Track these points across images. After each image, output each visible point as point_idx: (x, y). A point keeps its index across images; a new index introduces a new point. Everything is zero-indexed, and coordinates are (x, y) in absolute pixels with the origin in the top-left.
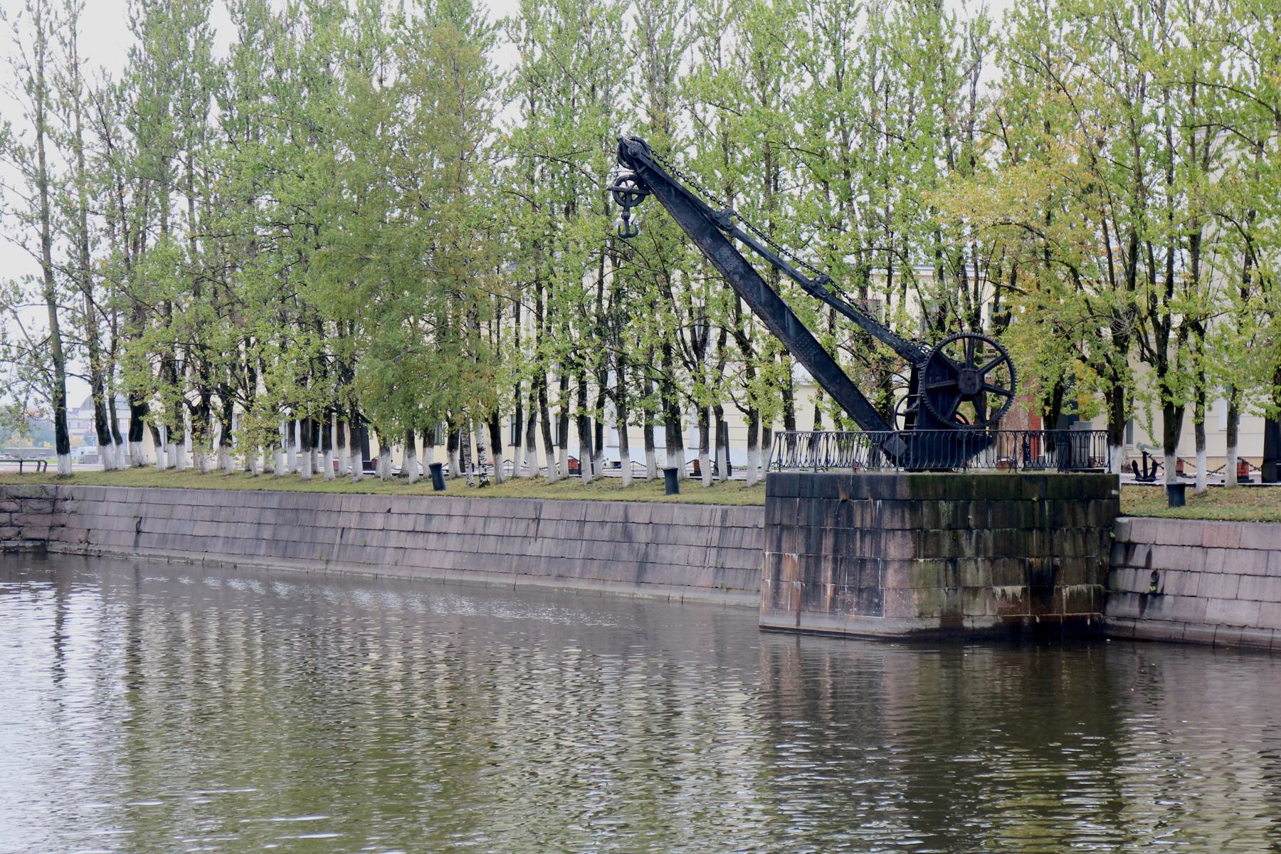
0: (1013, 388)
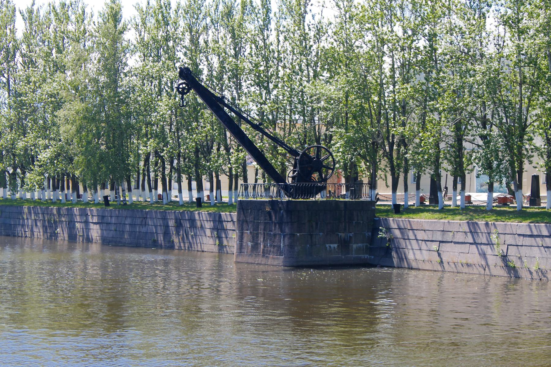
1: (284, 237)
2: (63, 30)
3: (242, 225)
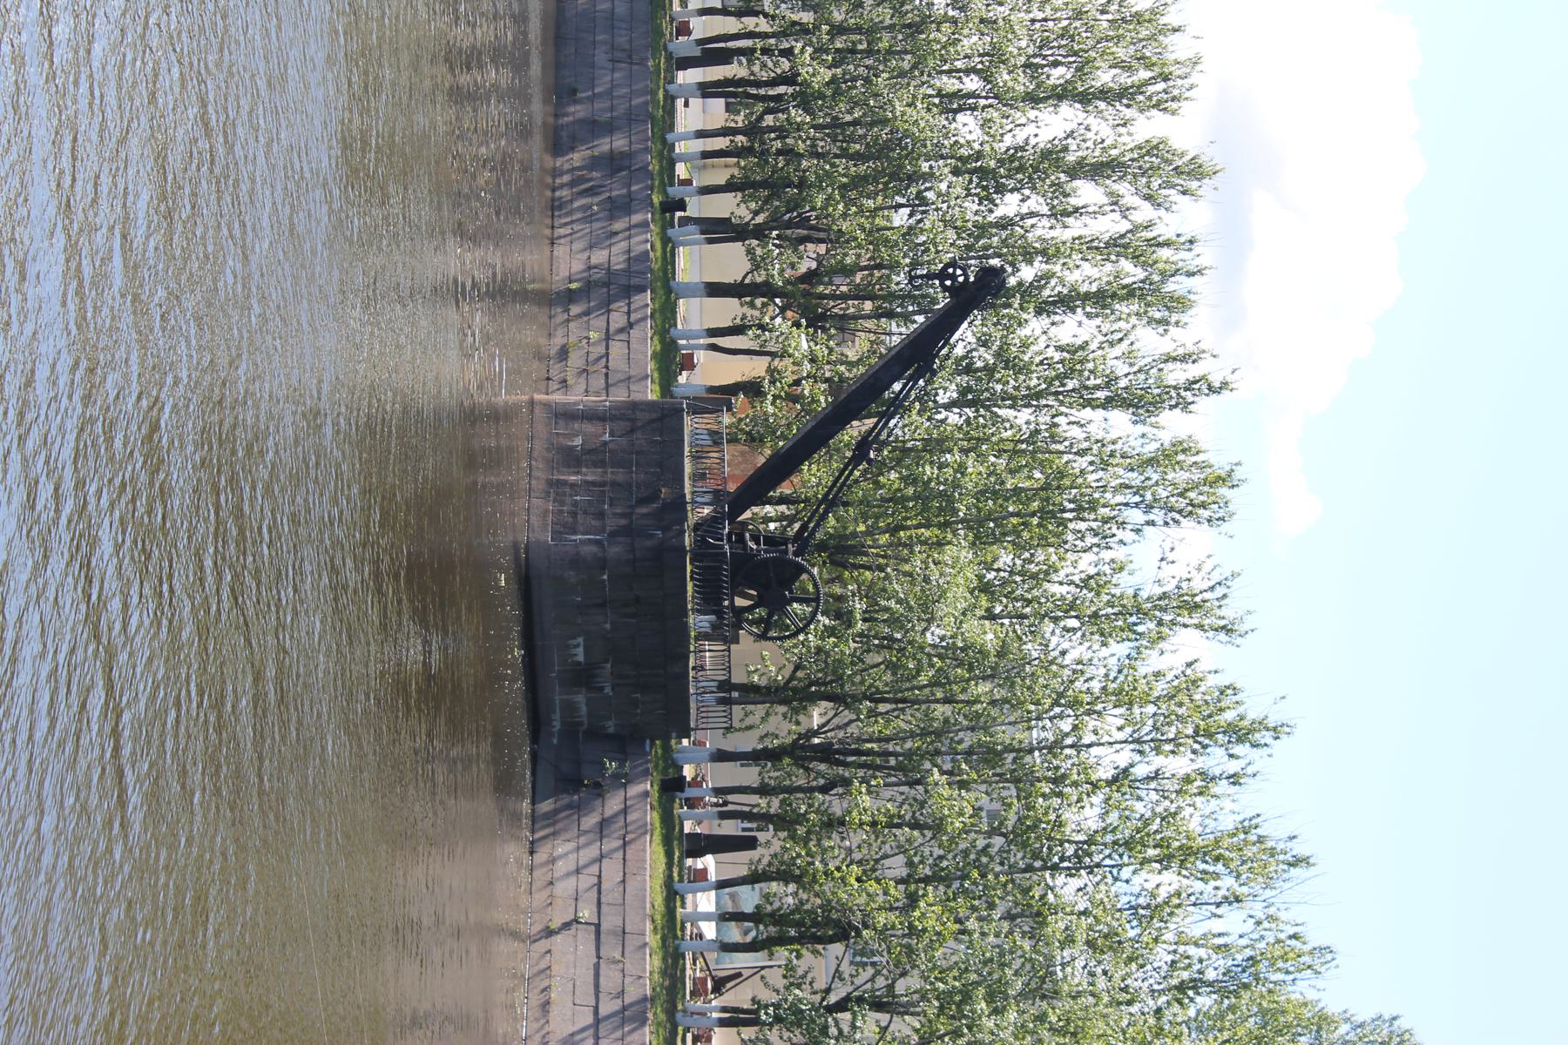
0: (772, 639)
1: (597, 542)
3: (622, 418)
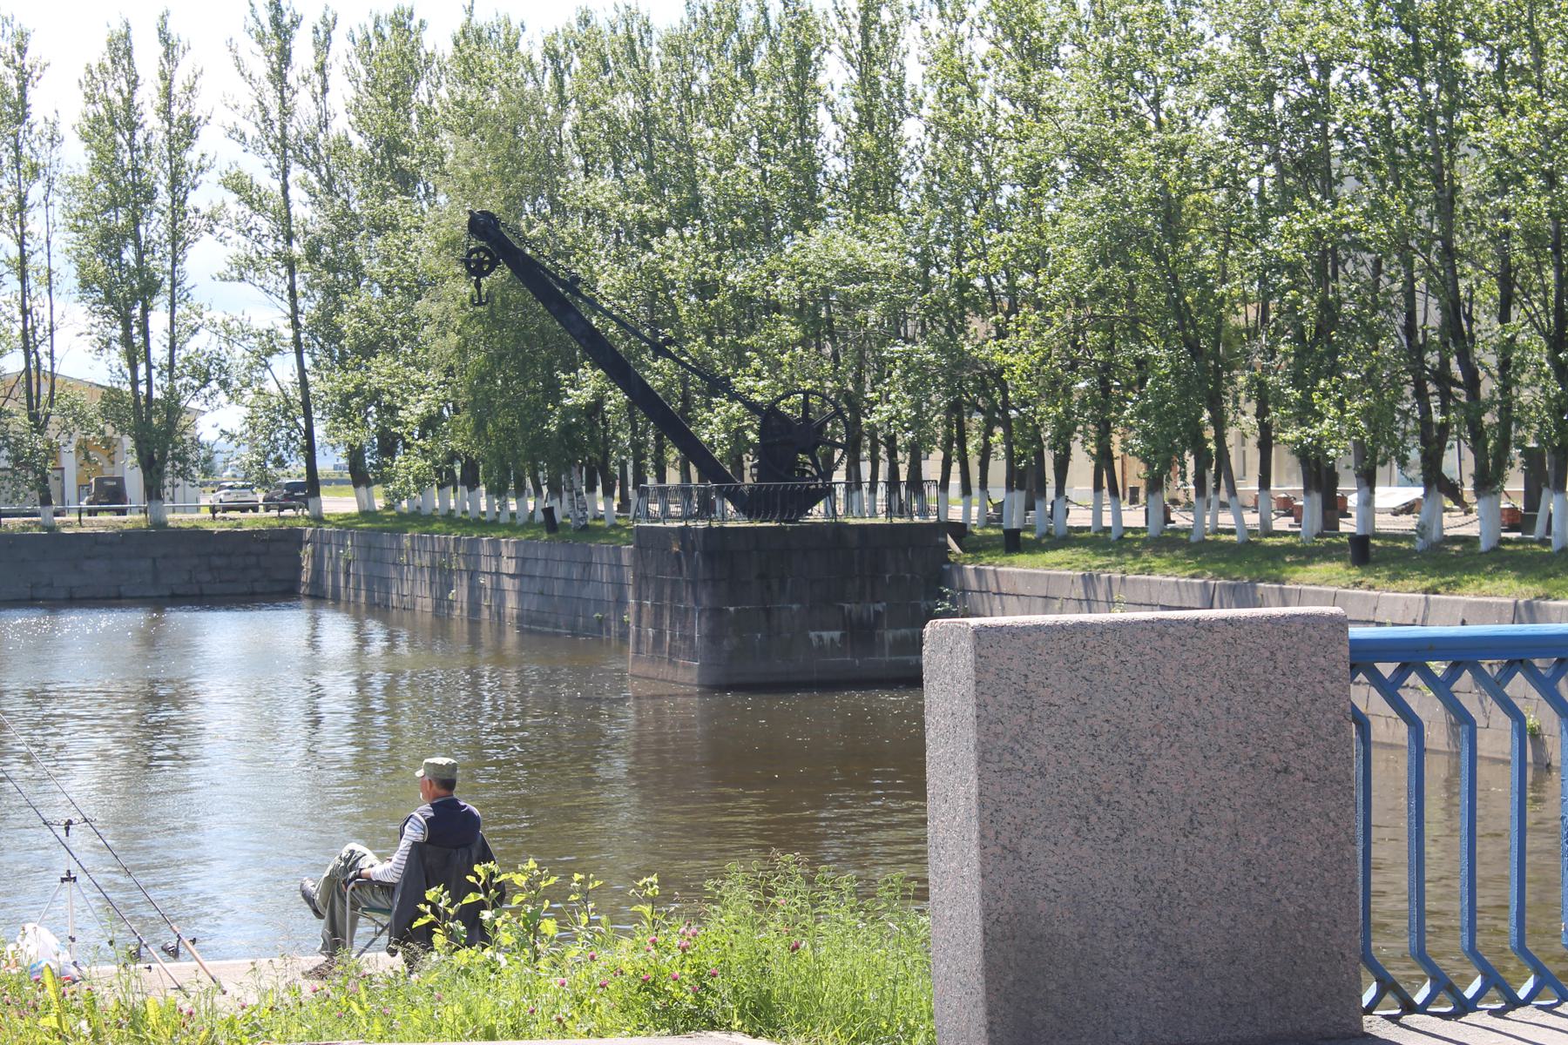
2: (459, 98)
